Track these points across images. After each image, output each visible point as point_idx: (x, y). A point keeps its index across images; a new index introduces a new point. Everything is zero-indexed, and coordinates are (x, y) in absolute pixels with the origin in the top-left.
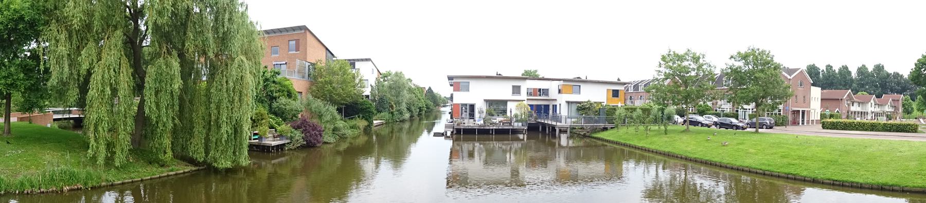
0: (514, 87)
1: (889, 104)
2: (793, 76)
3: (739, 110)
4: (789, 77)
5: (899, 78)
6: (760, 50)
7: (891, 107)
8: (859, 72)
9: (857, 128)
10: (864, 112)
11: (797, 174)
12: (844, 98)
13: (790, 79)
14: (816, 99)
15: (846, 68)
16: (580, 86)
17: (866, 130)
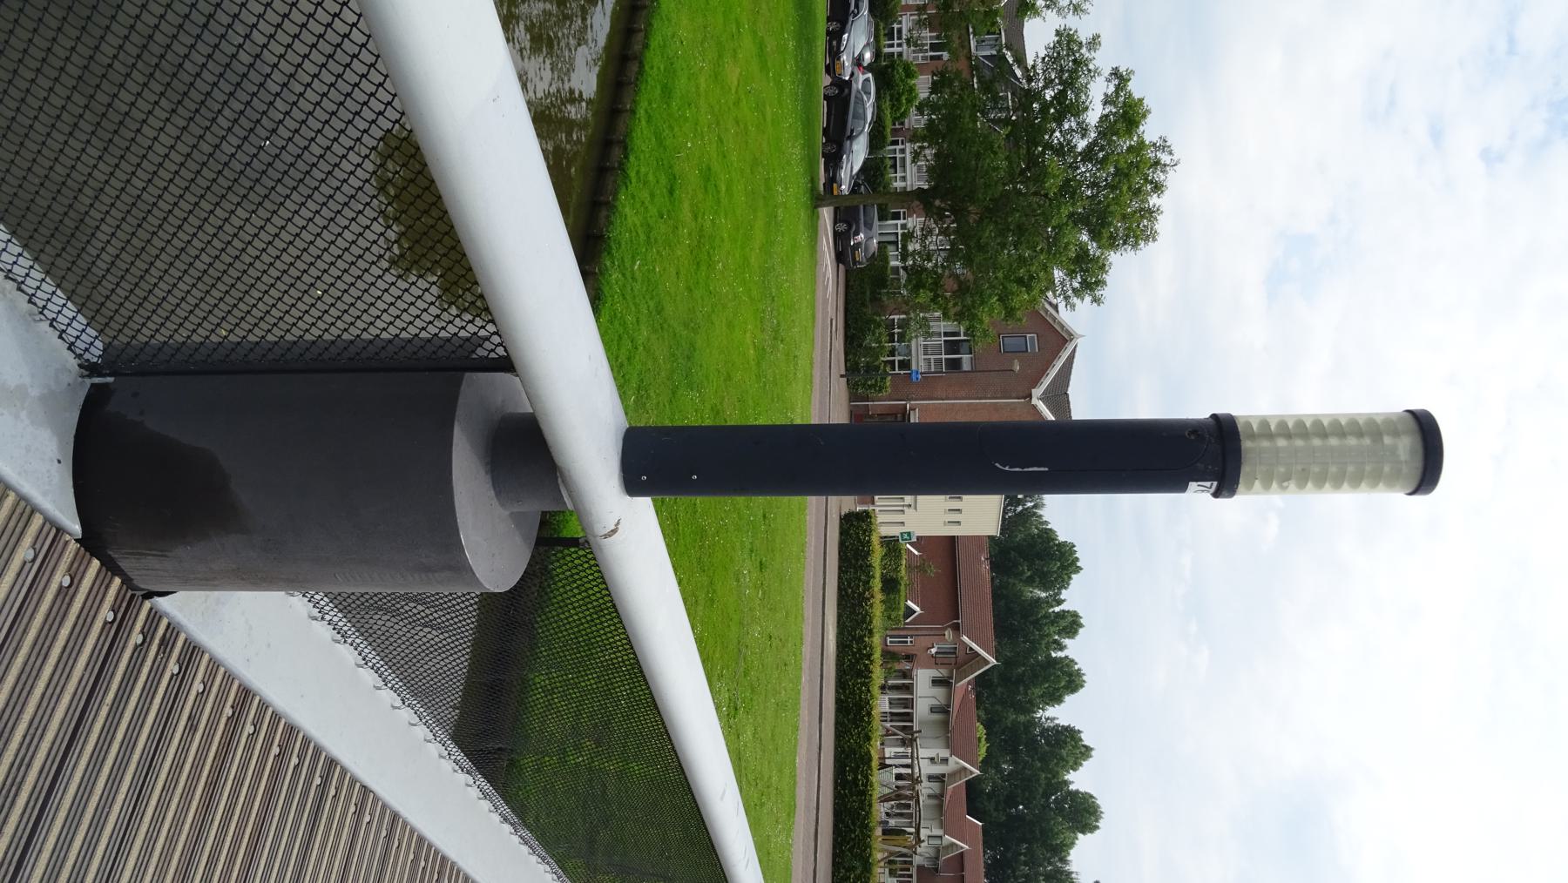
1: (948, 839)
3: (900, 222)
4: (1037, 392)
7: (932, 853)
9: (850, 647)
11: (626, 176)
12: (965, 638)
13: (1030, 396)
14: (955, 517)
17: (841, 684)
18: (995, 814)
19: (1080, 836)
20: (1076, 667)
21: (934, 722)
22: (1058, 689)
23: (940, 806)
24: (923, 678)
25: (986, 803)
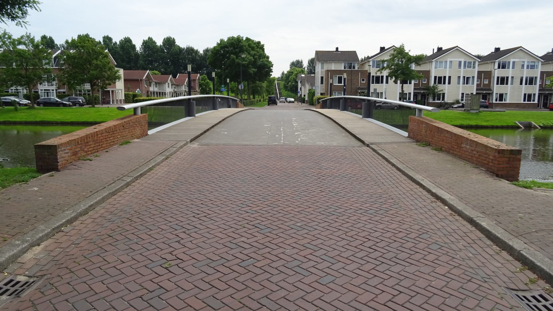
1: (169, 81)
5: (194, 54)
8: (145, 47)
10: (162, 93)
12: (144, 78)
15: (128, 41)
18: (171, 69)
19: (176, 44)
20: (123, 39)
21: (159, 86)
23: (159, 83)
24: (151, 89)
25: (168, 71)
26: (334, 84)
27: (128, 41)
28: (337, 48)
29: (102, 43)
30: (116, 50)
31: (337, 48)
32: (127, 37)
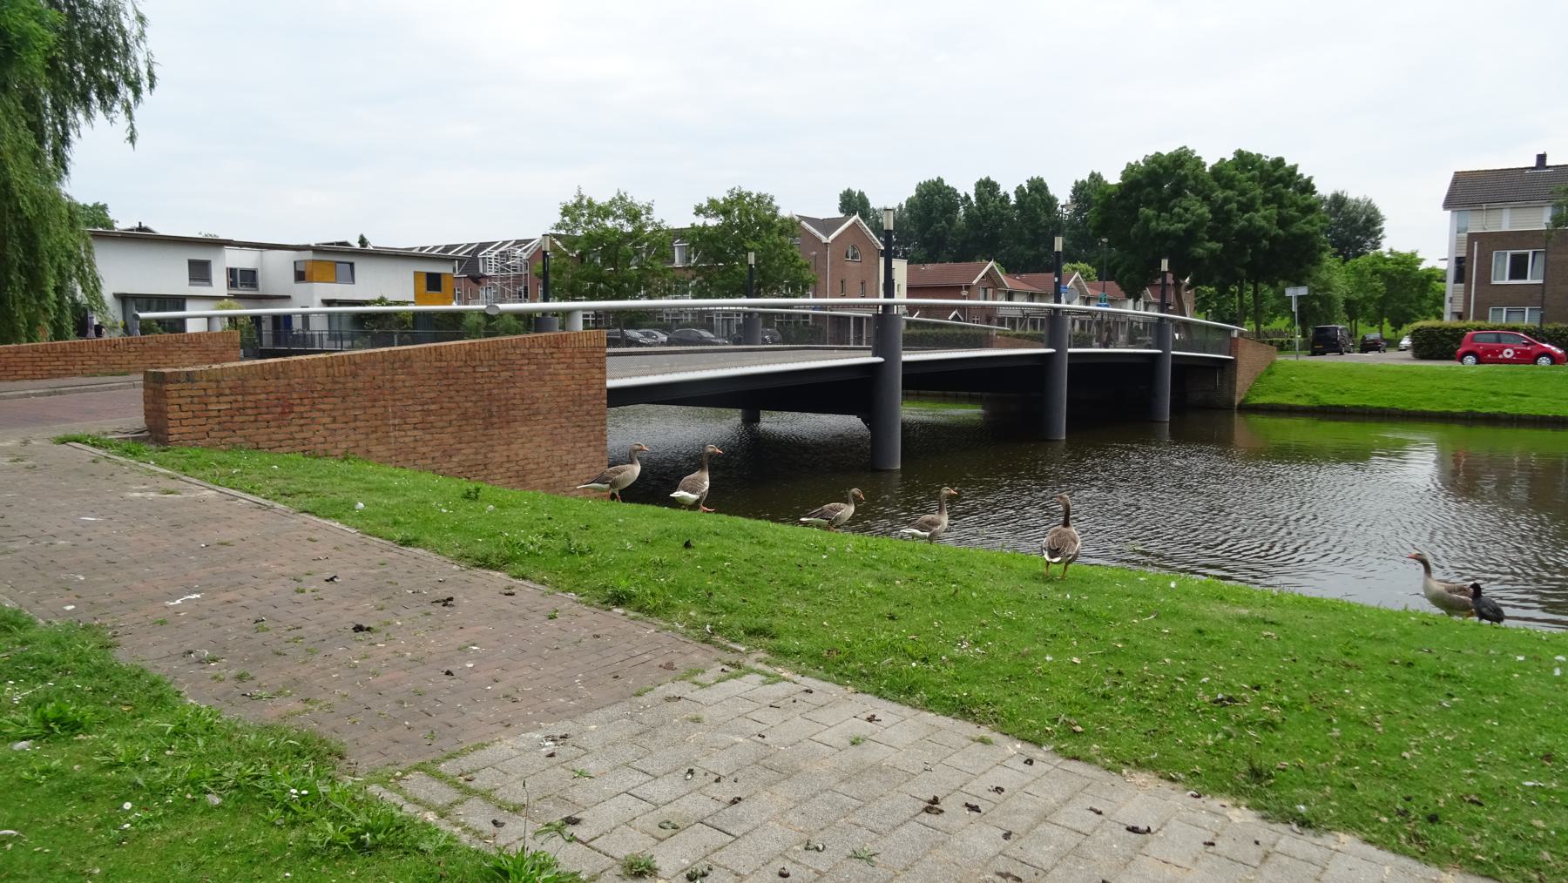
0: (192, 263)
2: (832, 237)
4: (824, 240)
6: (754, 196)
12: (975, 282)
13: (826, 244)
15: (1038, 186)
16: (352, 265)
22: (1042, 200)
26: (1494, 282)
27: (1038, 186)
28: (1542, 158)
29: (973, 199)
30: (1003, 215)
31: (1542, 158)
32: (1035, 177)
